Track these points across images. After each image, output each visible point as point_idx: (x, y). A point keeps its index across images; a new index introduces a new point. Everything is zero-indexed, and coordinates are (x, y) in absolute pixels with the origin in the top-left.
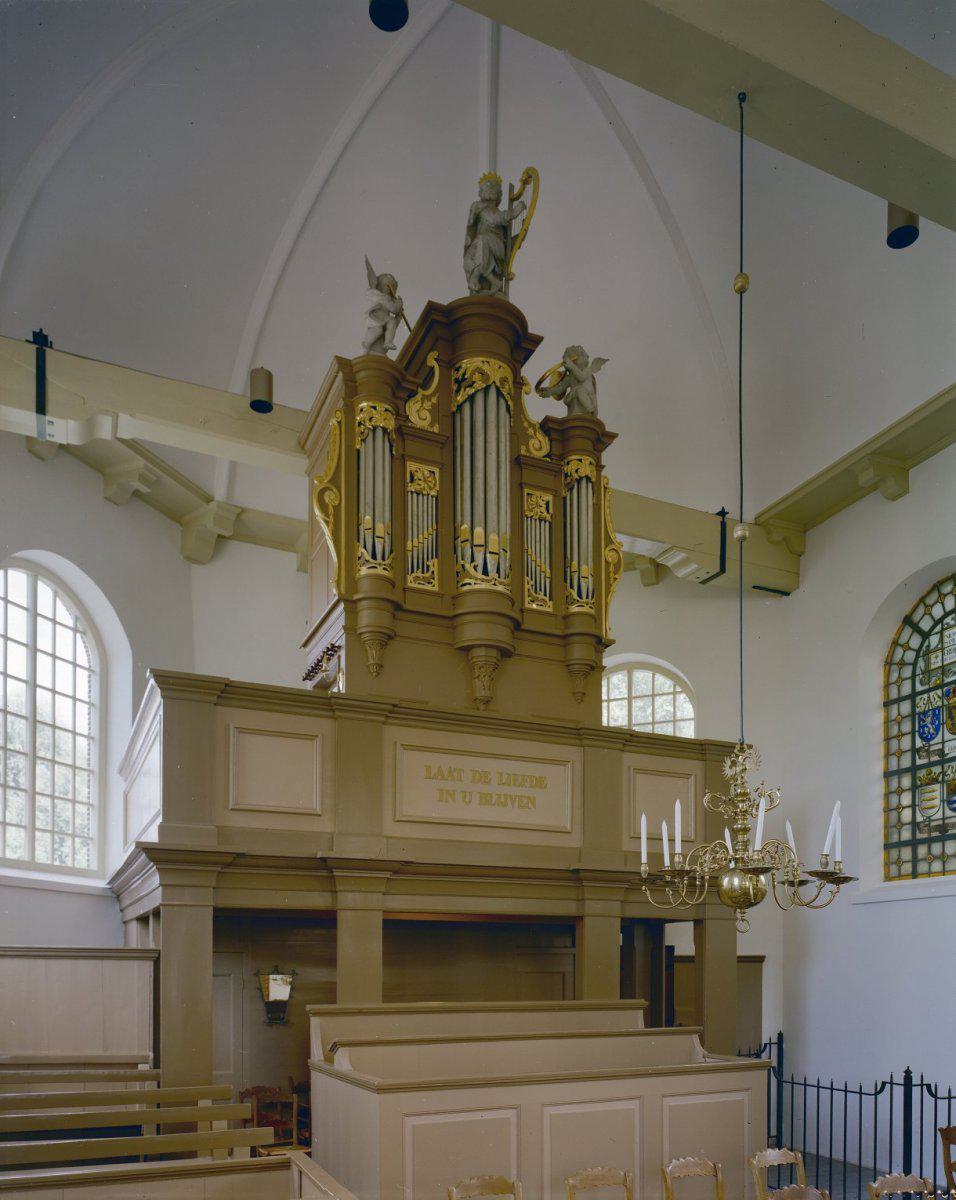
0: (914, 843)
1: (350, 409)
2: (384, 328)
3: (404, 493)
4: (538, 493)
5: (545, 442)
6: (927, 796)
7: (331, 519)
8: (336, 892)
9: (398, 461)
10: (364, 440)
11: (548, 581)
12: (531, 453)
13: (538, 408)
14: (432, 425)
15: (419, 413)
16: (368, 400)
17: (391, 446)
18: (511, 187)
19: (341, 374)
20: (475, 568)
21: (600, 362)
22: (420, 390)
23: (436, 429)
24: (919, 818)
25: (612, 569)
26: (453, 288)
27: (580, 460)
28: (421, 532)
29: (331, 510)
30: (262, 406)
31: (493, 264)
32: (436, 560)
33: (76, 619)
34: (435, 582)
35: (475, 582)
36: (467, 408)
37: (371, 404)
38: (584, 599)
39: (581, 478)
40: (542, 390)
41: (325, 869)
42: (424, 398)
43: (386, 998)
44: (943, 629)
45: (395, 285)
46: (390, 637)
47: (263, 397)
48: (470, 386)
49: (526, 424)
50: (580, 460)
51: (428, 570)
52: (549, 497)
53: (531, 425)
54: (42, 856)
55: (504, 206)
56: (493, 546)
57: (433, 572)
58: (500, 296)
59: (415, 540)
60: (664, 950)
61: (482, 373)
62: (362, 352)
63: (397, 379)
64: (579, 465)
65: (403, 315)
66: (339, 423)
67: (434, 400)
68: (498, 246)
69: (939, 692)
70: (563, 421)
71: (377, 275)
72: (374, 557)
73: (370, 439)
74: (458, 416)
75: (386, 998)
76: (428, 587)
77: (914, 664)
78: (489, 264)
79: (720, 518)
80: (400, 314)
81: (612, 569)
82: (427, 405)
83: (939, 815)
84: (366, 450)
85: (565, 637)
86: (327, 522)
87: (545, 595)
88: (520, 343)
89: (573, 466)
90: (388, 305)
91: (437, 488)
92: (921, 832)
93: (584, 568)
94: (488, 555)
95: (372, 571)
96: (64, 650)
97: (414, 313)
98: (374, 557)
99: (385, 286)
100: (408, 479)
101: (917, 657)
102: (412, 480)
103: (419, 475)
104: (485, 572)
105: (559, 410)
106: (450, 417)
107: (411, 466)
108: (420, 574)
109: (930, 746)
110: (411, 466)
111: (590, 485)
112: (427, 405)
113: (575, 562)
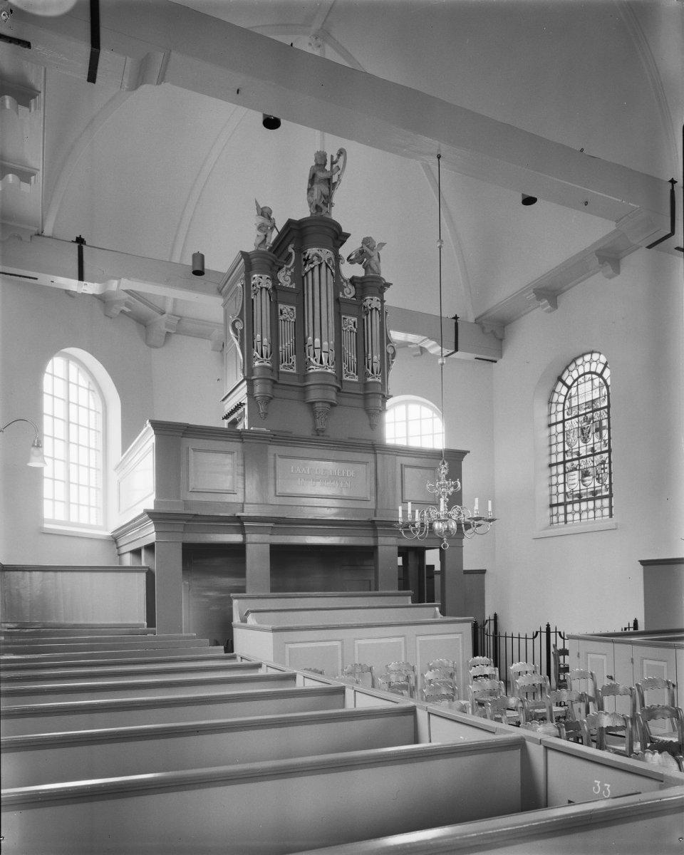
1: (248, 278)
2: (266, 236)
4: (348, 318)
5: (353, 289)
6: (572, 477)
9: (274, 305)
13: (351, 271)
14: (291, 284)
15: (285, 278)
16: (258, 273)
17: (270, 297)
18: (332, 156)
20: (316, 360)
21: (382, 245)
23: (293, 286)
24: (568, 490)
25: (390, 356)
26: (302, 211)
27: (372, 299)
29: (239, 332)
34: (295, 368)
36: (310, 274)
39: (372, 310)
42: (287, 269)
43: (399, 589)
45: (271, 212)
46: (271, 398)
47: (198, 268)
48: (312, 263)
49: (342, 280)
52: (355, 319)
53: (345, 281)
54: (73, 519)
55: (328, 167)
56: (325, 349)
58: (327, 216)
59: (283, 346)
64: (372, 302)
66: (242, 285)
67: (292, 270)
68: (326, 191)
72: (262, 356)
75: (273, 590)
76: (291, 371)
77: (564, 404)
79: (454, 321)
81: (390, 356)
84: (257, 300)
88: (339, 237)
90: (267, 222)
91: (295, 317)
94: (323, 354)
96: (83, 401)
98: (262, 356)
100: (279, 314)
101: (565, 400)
103: (284, 311)
104: (321, 362)
106: (300, 278)
107: (281, 306)
108: (287, 364)
110: (281, 306)
112: (289, 273)
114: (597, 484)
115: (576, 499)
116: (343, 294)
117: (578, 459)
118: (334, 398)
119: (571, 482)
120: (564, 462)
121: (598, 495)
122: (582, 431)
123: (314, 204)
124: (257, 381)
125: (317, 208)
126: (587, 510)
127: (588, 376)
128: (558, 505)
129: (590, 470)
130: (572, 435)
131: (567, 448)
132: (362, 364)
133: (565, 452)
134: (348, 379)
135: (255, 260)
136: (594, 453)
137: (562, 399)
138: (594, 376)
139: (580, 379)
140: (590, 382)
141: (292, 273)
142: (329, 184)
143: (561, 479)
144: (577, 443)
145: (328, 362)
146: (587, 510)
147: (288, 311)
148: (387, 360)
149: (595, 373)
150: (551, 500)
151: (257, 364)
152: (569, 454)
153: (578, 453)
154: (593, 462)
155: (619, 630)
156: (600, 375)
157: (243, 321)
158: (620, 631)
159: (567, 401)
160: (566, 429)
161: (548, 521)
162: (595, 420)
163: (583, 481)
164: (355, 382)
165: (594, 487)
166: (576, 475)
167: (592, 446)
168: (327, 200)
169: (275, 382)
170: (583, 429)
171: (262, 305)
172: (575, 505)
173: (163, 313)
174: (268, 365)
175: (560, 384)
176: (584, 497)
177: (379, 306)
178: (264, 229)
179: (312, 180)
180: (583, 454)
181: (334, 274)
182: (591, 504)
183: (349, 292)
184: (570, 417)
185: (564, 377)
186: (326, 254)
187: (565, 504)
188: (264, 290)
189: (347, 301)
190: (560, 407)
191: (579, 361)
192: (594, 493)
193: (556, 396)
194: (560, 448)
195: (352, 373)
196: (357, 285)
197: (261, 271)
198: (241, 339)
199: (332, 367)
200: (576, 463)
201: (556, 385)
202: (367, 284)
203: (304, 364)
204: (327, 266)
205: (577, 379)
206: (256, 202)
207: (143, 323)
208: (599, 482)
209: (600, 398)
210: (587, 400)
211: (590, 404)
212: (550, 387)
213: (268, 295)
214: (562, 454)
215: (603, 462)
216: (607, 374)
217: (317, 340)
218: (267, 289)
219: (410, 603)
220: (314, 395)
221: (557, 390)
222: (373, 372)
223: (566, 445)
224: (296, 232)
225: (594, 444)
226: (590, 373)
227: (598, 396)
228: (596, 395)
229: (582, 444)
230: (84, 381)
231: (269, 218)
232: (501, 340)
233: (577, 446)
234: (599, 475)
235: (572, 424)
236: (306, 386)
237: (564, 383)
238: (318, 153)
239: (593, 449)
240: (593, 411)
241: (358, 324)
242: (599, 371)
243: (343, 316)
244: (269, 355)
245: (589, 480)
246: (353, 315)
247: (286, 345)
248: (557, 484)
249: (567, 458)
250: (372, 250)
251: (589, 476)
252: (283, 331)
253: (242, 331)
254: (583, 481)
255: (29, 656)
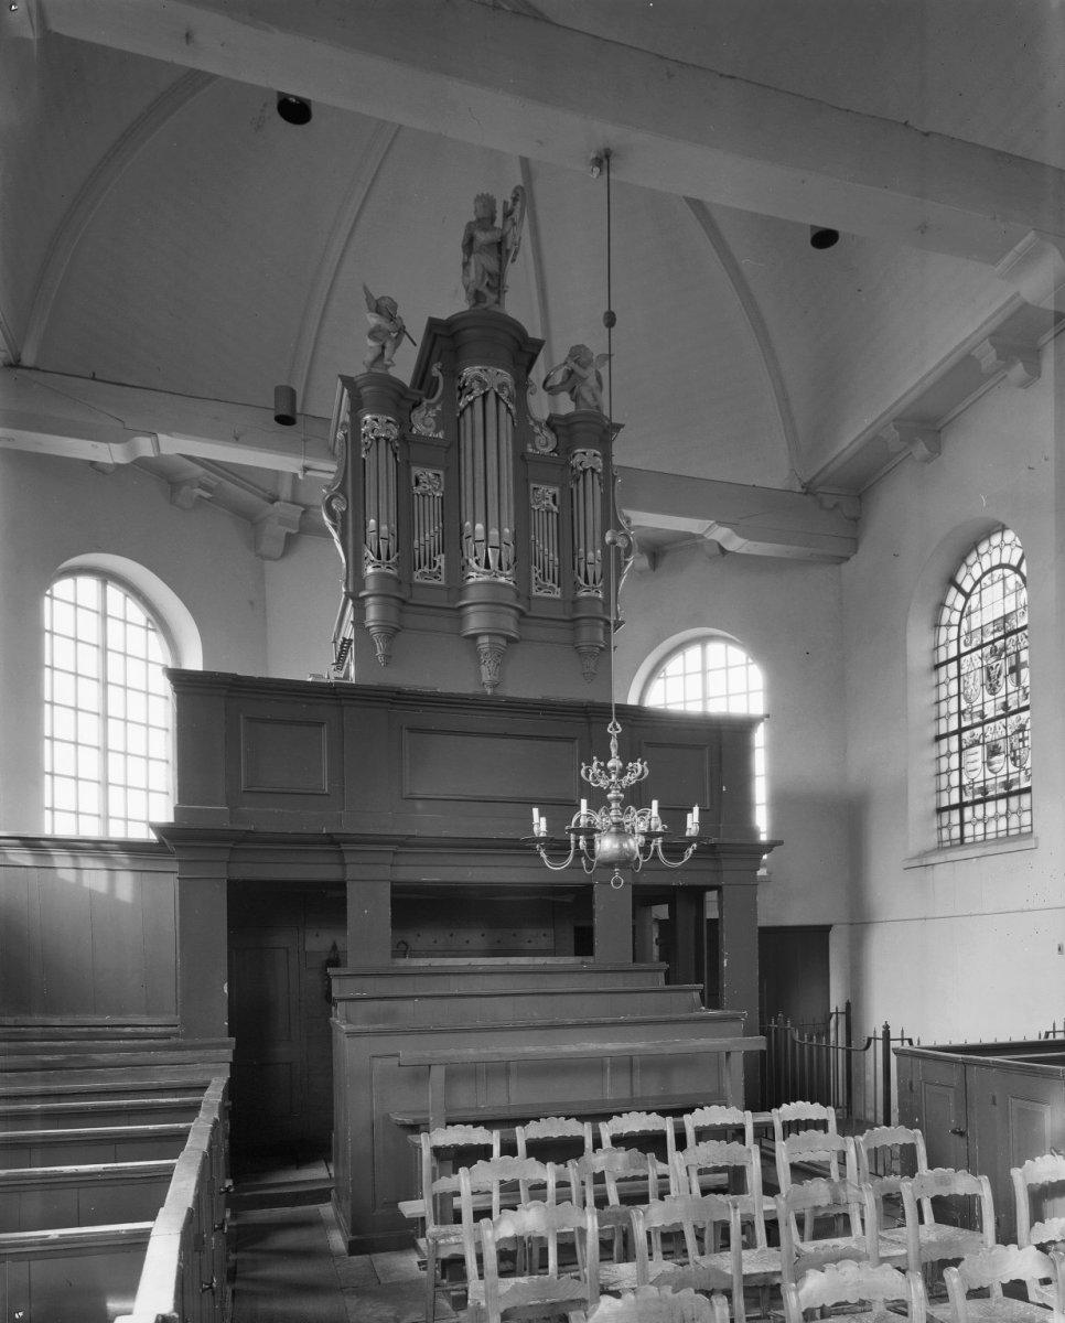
0: (961, 806)
2: (383, 347)
3: (411, 496)
4: (543, 488)
5: (551, 437)
6: (972, 758)
7: (339, 525)
8: (345, 865)
9: (403, 471)
10: (367, 450)
11: (556, 568)
12: (537, 450)
13: (541, 406)
14: (436, 431)
15: (424, 423)
16: (371, 413)
17: (395, 455)
18: (505, 203)
19: (346, 390)
20: (477, 562)
22: (424, 399)
23: (440, 435)
24: (965, 781)
25: (622, 553)
26: (451, 304)
27: (584, 453)
28: (422, 533)
29: (339, 517)
30: (285, 420)
31: (487, 280)
32: (443, 556)
33: (148, 620)
34: (442, 577)
35: (476, 575)
36: (468, 412)
37: (374, 416)
38: (591, 584)
39: (585, 471)
40: (551, 388)
41: (334, 843)
42: (430, 406)
44: (982, 589)
45: (395, 306)
46: (397, 630)
47: (284, 411)
48: (470, 393)
49: (532, 423)
50: (584, 453)
51: (435, 565)
52: (556, 490)
53: (538, 423)
55: (498, 223)
56: (494, 541)
57: (440, 567)
58: (496, 308)
59: (422, 538)
60: (705, 926)
61: (480, 380)
62: (364, 370)
63: (400, 394)
64: (586, 457)
65: (405, 332)
66: (345, 435)
67: (439, 408)
68: (492, 265)
69: (979, 652)
70: (568, 417)
71: (376, 298)
72: (379, 557)
73: (373, 449)
74: (462, 421)
76: (435, 582)
77: (959, 626)
78: (483, 280)
80: (402, 331)
81: (622, 553)
82: (432, 413)
83: (981, 778)
85: (574, 620)
86: (334, 527)
87: (554, 582)
88: (522, 351)
89: (578, 459)
90: (387, 325)
91: (442, 489)
92: (966, 795)
93: (590, 554)
94: (489, 550)
95: (377, 570)
96: (136, 648)
97: (417, 330)
98: (379, 557)
99: (386, 309)
100: (414, 483)
101: (961, 618)
102: (417, 483)
104: (487, 566)
105: (566, 405)
106: (453, 422)
107: (416, 471)
108: (426, 569)
109: (972, 707)
110: (416, 471)
111: (596, 476)
112: (432, 413)
113: (582, 550)
114: (1012, 769)
115: (979, 796)
116: (534, 447)
117: (981, 724)
118: (512, 627)
119: (971, 766)
120: (960, 731)
121: (1015, 788)
122: (989, 674)
123: (471, 289)
124: (371, 600)
125: (477, 297)
126: (996, 817)
127: (998, 573)
128: (951, 808)
129: (1001, 743)
130: (971, 681)
131: (964, 706)
132: (568, 569)
133: (961, 713)
134: (541, 593)
135: (365, 390)
136: (1007, 712)
137: (955, 617)
138: (1008, 572)
139: (986, 580)
140: (1001, 583)
141: (438, 412)
142: (500, 252)
143: (955, 760)
144: (981, 697)
145: (500, 565)
146: (996, 817)
147: (429, 479)
148: (614, 559)
149: (1008, 566)
150: (939, 800)
151: (370, 570)
152: (968, 716)
153: (982, 715)
154: (1006, 728)
155: (1033, 1037)
156: (1017, 570)
157: (346, 497)
158: (1036, 1038)
159: (964, 620)
160: (963, 672)
161: (934, 838)
162: (1008, 652)
163: (990, 764)
164: (554, 600)
165: (1008, 775)
166: (977, 755)
167: (1004, 699)
168: (497, 281)
169: (404, 602)
170: (989, 669)
171: (381, 469)
172: (987, 804)
173: (273, 499)
174: (390, 572)
175: (953, 591)
176: (991, 793)
177: (599, 464)
178: (380, 335)
179: (469, 245)
180: (990, 714)
181: (514, 412)
182: (1002, 804)
183: (544, 443)
184: (969, 648)
185: (959, 580)
186: (500, 376)
187: (961, 806)
188: (382, 442)
189: (542, 460)
190: (953, 632)
191: (983, 548)
192: (1007, 785)
193: (946, 612)
194: (953, 707)
195: (549, 584)
196: (559, 430)
197: (378, 409)
198: (342, 528)
199: (508, 573)
200: (978, 731)
201: (946, 593)
202: (577, 426)
203: (459, 569)
204: (498, 397)
205: (979, 581)
206: (365, 288)
207: (249, 521)
208: (1015, 765)
209: (1017, 610)
210: (995, 618)
211: (1001, 622)
212: (935, 600)
213: (391, 453)
214: (956, 716)
215: (1022, 729)
216: (1024, 569)
217: (480, 527)
218: (387, 440)
219: (661, 984)
220: (475, 622)
221: (948, 602)
222: (586, 581)
223: (963, 701)
224: (445, 340)
225: (1007, 695)
226: (1001, 566)
227: (1014, 608)
228: (1010, 608)
229: (988, 697)
230: (137, 613)
231: (392, 318)
232: (856, 520)
233: (979, 701)
234: (1015, 751)
235: (972, 663)
236: (462, 607)
237: (960, 589)
238: (479, 198)
239: (1005, 706)
240: (1005, 637)
241: (561, 500)
242: (1015, 563)
243: (533, 485)
244: (598, 578)
245: (999, 761)
246: (554, 484)
247: (427, 536)
248: (949, 771)
249: (964, 724)
250: (585, 368)
251: (998, 754)
252: (551, 538)
253: (344, 514)
254: (990, 764)
255: (539, 961)
